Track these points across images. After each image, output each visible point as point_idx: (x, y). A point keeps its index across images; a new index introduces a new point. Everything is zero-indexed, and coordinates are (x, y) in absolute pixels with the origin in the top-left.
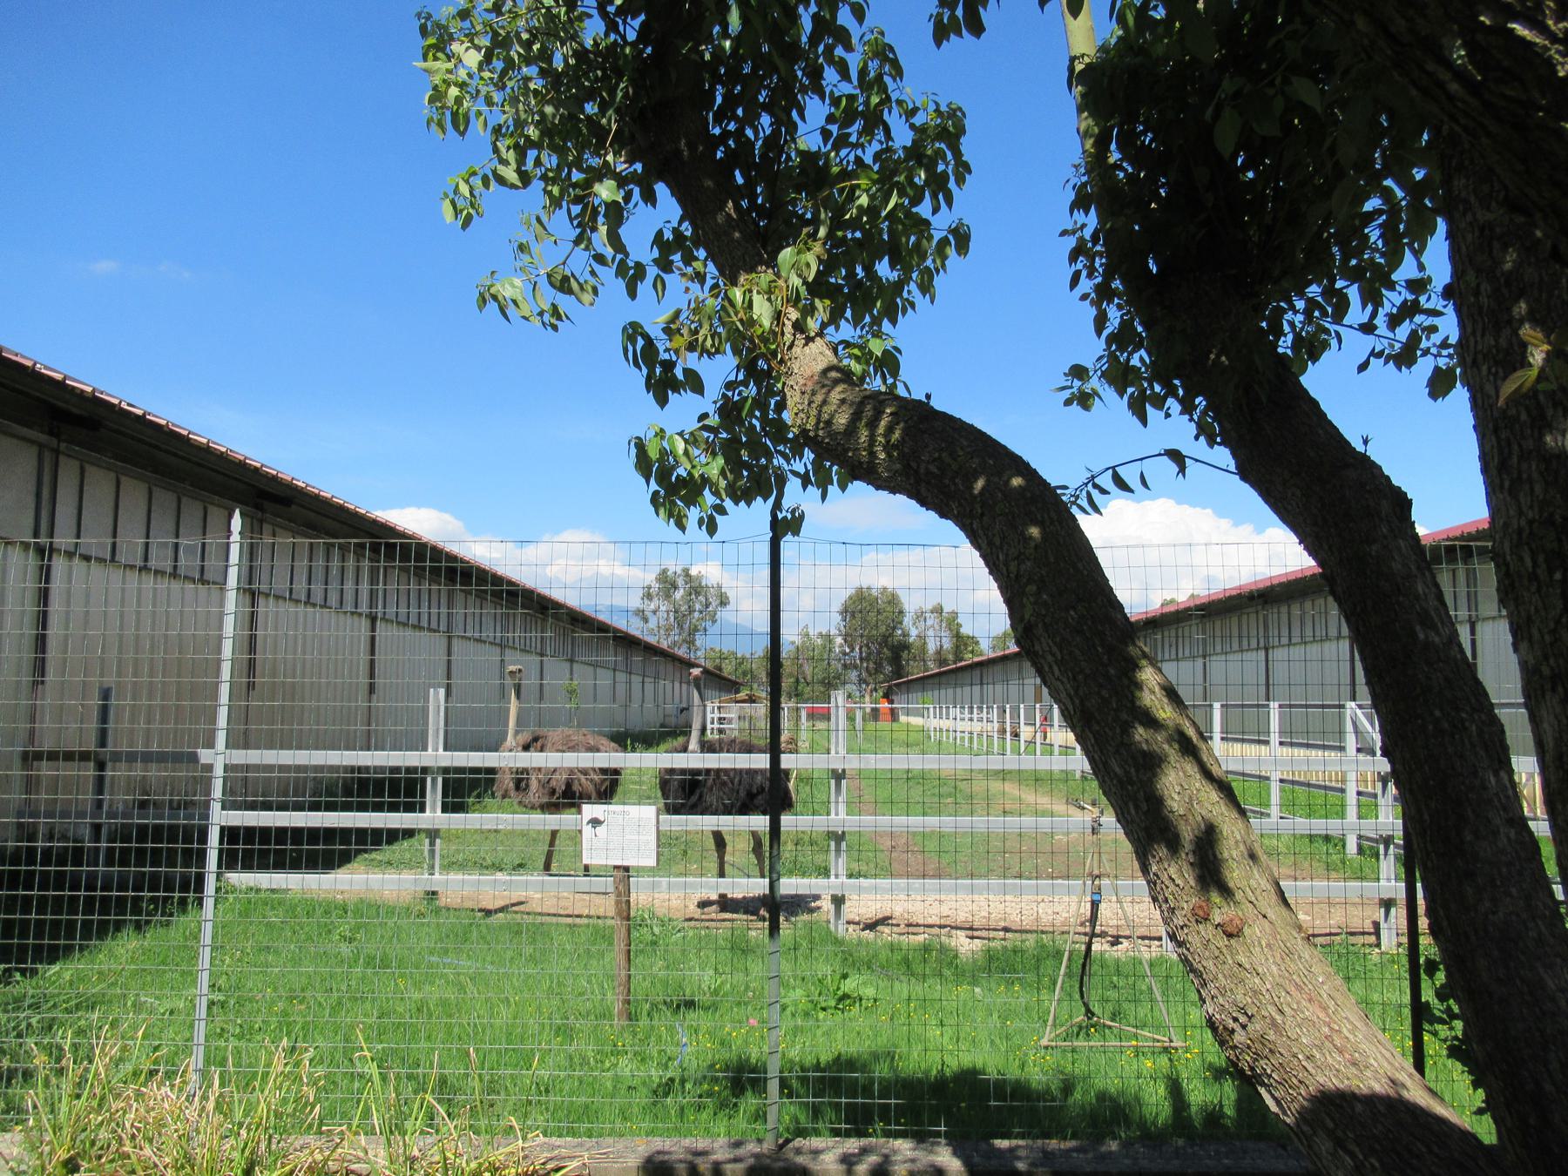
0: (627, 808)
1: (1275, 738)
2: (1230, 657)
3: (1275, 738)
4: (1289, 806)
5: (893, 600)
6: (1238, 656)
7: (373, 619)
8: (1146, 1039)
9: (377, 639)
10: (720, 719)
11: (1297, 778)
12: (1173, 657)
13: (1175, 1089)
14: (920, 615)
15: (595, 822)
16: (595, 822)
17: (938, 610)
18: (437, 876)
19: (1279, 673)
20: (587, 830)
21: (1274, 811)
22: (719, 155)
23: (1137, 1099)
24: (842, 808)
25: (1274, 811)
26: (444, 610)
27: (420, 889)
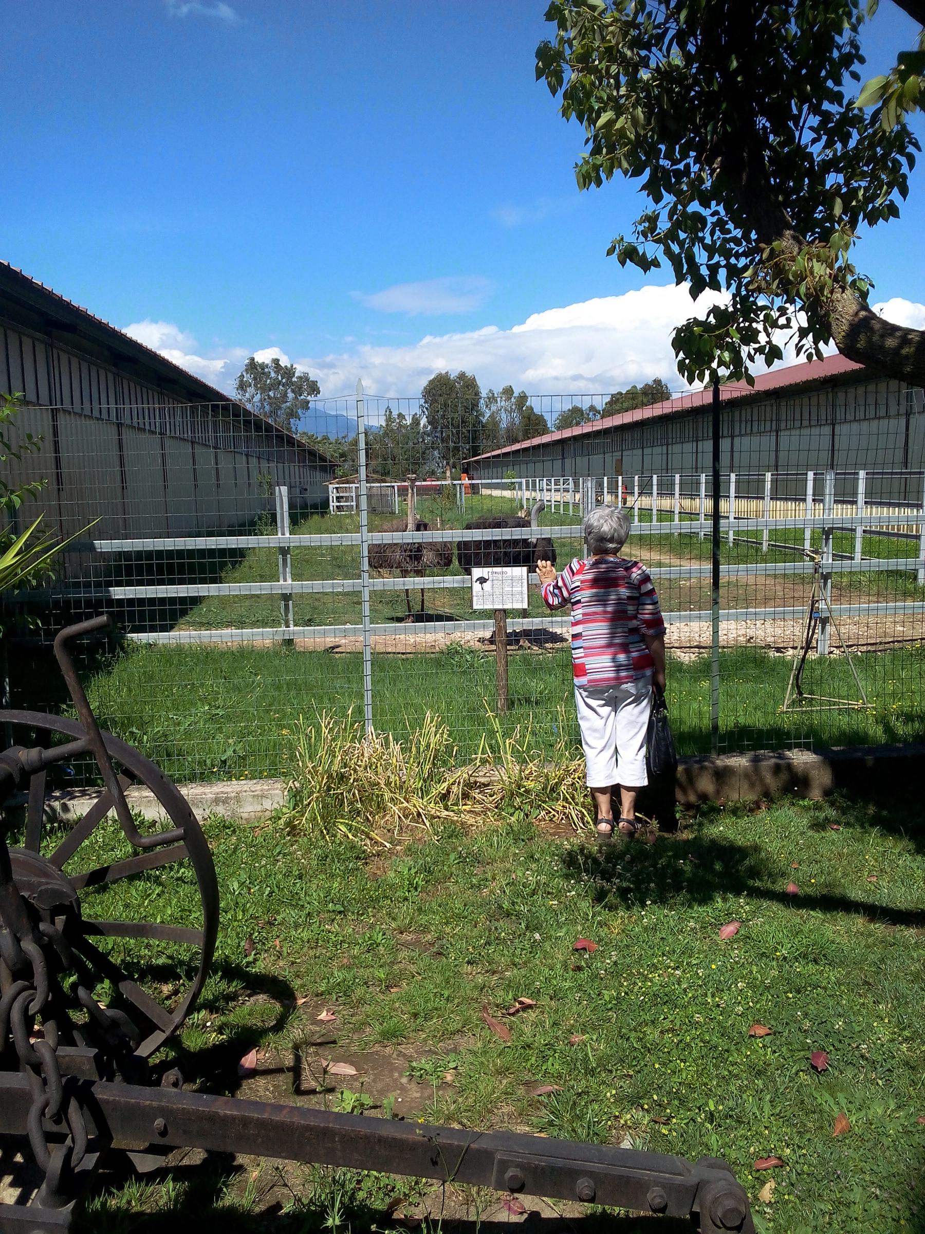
0: (505, 569)
1: (861, 498)
2: (793, 432)
3: (861, 498)
4: (868, 551)
5: (468, 384)
6: (798, 432)
7: (119, 425)
8: (844, 704)
9: (124, 441)
10: (337, 498)
11: (873, 529)
12: (749, 431)
13: (888, 729)
14: (492, 399)
15: (482, 580)
16: (482, 580)
17: (508, 391)
18: (292, 628)
19: (842, 443)
20: (477, 587)
21: (858, 556)
22: (903, 67)
23: (866, 733)
24: (288, 576)
25: (858, 556)
26: (112, 406)
27: (279, 638)
